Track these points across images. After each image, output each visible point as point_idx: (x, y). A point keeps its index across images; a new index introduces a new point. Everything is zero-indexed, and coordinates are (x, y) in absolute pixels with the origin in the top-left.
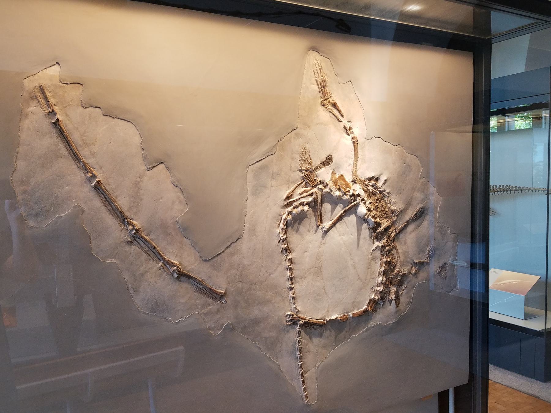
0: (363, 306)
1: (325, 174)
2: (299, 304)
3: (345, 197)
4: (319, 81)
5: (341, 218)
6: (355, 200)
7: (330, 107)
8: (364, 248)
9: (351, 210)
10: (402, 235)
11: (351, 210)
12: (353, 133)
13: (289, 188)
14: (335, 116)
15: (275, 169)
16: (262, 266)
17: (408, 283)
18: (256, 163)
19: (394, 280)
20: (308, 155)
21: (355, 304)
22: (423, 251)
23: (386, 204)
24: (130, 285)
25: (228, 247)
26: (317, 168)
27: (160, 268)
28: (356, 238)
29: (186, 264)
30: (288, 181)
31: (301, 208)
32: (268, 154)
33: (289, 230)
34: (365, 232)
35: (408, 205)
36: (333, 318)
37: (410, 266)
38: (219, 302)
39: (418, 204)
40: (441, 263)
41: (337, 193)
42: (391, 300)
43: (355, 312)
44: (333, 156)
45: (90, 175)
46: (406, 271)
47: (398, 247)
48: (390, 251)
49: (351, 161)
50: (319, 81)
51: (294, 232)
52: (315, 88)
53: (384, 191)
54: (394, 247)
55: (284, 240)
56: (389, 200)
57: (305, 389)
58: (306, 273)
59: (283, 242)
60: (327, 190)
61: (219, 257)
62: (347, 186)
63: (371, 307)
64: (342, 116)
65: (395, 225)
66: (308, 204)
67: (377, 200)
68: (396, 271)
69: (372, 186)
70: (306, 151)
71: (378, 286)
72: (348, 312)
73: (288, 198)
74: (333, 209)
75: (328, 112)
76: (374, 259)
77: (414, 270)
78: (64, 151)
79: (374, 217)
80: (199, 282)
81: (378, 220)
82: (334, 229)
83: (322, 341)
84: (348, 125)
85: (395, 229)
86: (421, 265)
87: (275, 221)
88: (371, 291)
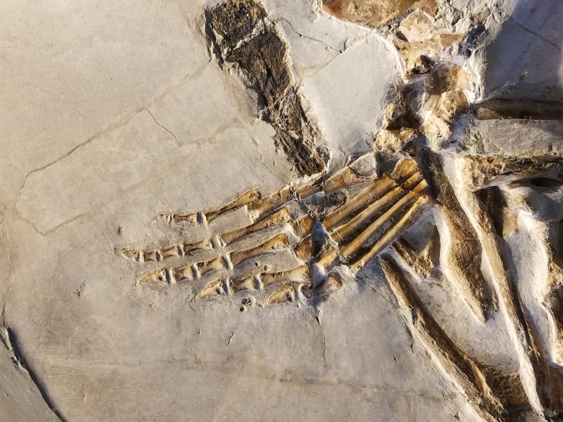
13: (438, 397)
20: (205, 233)
26: (302, 156)
30: (389, 399)
60: (470, 79)
70: (176, 242)
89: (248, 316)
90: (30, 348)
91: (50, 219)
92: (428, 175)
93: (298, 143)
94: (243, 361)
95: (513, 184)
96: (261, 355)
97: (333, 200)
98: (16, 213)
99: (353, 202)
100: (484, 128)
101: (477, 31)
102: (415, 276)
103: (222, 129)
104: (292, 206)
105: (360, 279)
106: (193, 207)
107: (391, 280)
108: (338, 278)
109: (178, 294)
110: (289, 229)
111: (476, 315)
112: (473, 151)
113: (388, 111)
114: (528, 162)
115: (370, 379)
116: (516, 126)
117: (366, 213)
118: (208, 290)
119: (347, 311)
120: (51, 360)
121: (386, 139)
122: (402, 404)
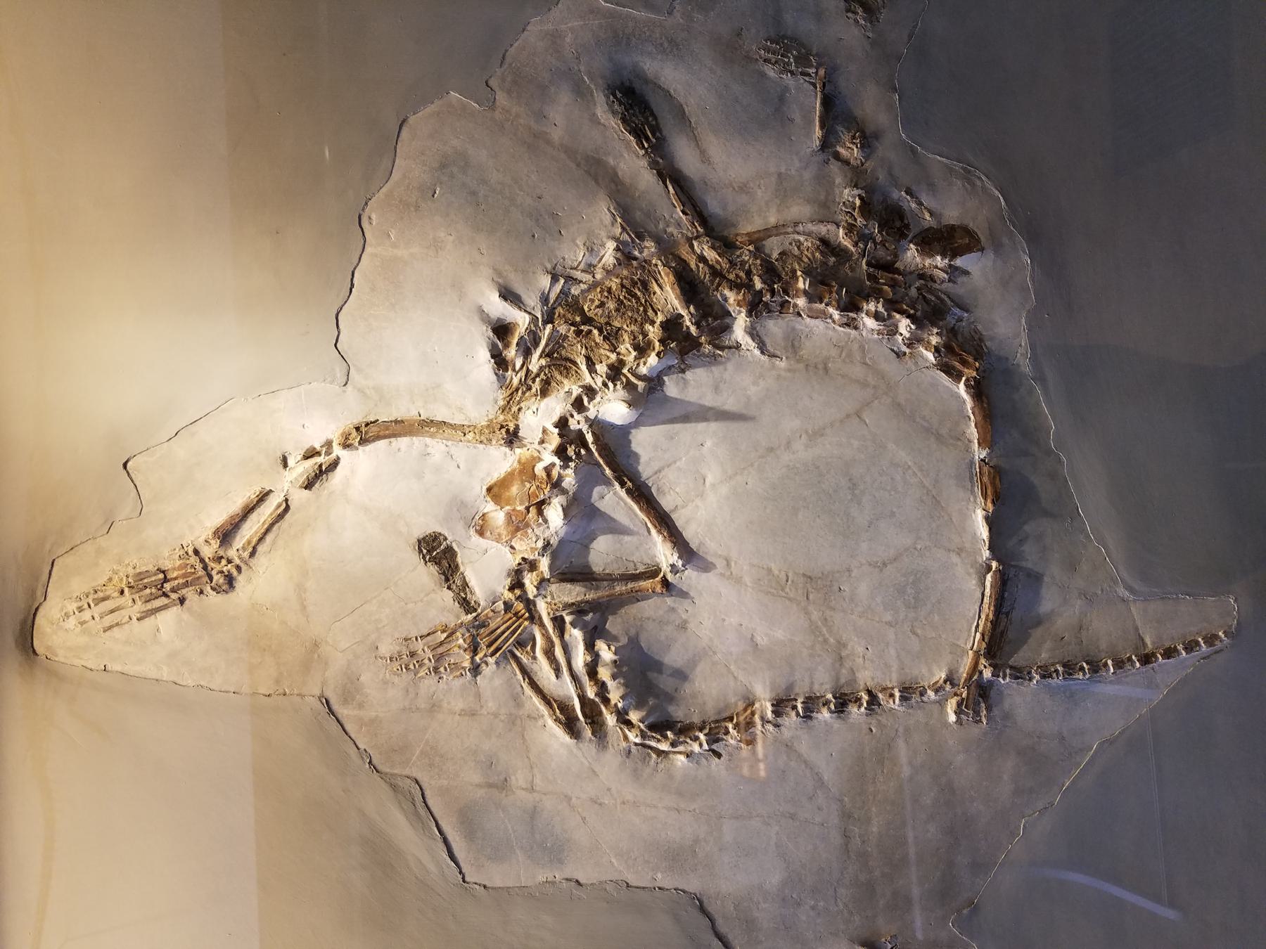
0: (958, 396)
1: (486, 567)
2: (924, 671)
3: (570, 480)
4: (140, 607)
5: (642, 495)
6: (580, 437)
7: (232, 553)
8: (753, 390)
9: (610, 454)
10: (713, 206)
11: (610, 454)
12: (329, 444)
14: (268, 531)
15: (472, 776)
16: (793, 817)
17: (897, 186)
18: (452, 856)
19: (881, 253)
20: (419, 646)
21: (944, 431)
26: (466, 605)
28: (713, 426)
30: (512, 720)
31: (604, 674)
32: (422, 811)
33: (678, 713)
34: (693, 385)
35: (598, 174)
36: (983, 532)
37: (834, 167)
39: (594, 120)
41: (554, 514)
42: (953, 271)
43: (973, 432)
44: (419, 532)
46: (850, 195)
48: (771, 272)
49: (436, 446)
50: (140, 607)
51: (687, 689)
52: (169, 620)
53: (545, 299)
54: (757, 240)
55: (713, 739)
56: (578, 274)
57: (1190, 647)
58: (826, 641)
60: (544, 564)
62: (526, 470)
63: (964, 363)
64: (263, 497)
65: (675, 244)
66: (590, 646)
67: (578, 333)
68: (847, 243)
69: (527, 353)
70: (405, 651)
71: (893, 331)
72: (972, 463)
73: (570, 725)
74: (615, 528)
75: (253, 562)
76: (793, 344)
77: (850, 151)
79: (642, 350)
81: (654, 332)
82: (679, 519)
83: (1054, 572)
84: (301, 469)
85: (689, 241)
86: (834, 112)
87: (648, 770)
88: (910, 363)
89: (442, 685)
90: (335, 707)
91: (344, 645)
92: (529, 611)
93: (465, 599)
94: (440, 707)
95: (571, 613)
96: (449, 703)
97: (483, 625)
98: (327, 642)
99: (493, 625)
100: (554, 587)
101: (547, 545)
102: (525, 659)
103: (427, 595)
104: (463, 630)
105: (497, 663)
106: (413, 634)
107: (515, 666)
108: (487, 664)
109: (407, 677)
110: (461, 641)
111: (553, 677)
112: (549, 599)
113: (508, 582)
114: (573, 604)
115: (503, 711)
116: (569, 586)
117: (499, 631)
118: (422, 674)
119: (491, 679)
120: (346, 712)
121: (508, 596)
122: (518, 722)
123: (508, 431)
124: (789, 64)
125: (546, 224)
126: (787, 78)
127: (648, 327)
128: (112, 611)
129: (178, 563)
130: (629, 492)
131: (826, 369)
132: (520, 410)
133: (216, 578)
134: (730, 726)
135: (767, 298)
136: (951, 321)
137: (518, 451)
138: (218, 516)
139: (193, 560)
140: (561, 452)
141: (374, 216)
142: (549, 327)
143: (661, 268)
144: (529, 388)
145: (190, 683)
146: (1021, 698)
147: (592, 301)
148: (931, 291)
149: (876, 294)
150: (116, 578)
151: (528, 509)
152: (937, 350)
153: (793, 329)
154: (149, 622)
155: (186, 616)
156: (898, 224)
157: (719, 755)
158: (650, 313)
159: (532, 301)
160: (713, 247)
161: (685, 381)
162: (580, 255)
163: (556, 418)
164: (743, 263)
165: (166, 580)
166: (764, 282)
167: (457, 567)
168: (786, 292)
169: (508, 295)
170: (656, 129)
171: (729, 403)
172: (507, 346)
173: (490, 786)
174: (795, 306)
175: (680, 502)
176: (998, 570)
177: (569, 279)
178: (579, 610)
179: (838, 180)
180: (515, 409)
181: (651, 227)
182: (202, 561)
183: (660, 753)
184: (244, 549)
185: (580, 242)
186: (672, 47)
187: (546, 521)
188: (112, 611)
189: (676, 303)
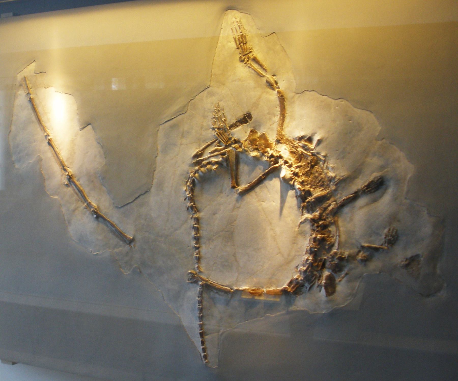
0: (283, 285)
10: (346, 210)
12: (278, 88)
13: (199, 146)
15: (186, 128)
22: (378, 234)
23: (322, 169)
24: (66, 217)
25: (137, 198)
26: (231, 127)
27: (85, 208)
29: (102, 207)
31: (209, 166)
32: (178, 114)
34: (292, 199)
37: (356, 250)
38: (128, 246)
40: (409, 253)
41: (254, 154)
42: (320, 286)
43: (272, 289)
45: (46, 134)
46: (346, 254)
47: (340, 223)
48: (325, 227)
52: (233, 45)
53: (318, 153)
56: (326, 164)
58: (214, 236)
59: (189, 199)
61: (129, 205)
62: (268, 145)
63: (293, 288)
64: (265, 70)
66: (217, 163)
67: (308, 163)
68: (332, 252)
74: (252, 170)
75: (247, 67)
76: (302, 233)
78: (34, 118)
79: (302, 183)
80: (112, 225)
81: (307, 188)
89: (210, 119)
99: (225, 134)
104: (224, 125)
105: (215, 135)
111: (210, 151)
113: (237, 139)
116: (235, 157)
121: (233, 139)
123: (280, 140)
124: (388, 237)
125: (342, 155)
126: (383, 236)
127: (309, 186)
128: (236, 30)
129: (248, 47)
130: (261, 177)
131: (294, 243)
132: (287, 144)
133: (243, 57)
134: (192, 204)
135: (316, 225)
136: (306, 284)
137: (274, 143)
138: (260, 57)
139: (248, 51)
140: (272, 156)
141: (343, 102)
142: (311, 154)
143: (327, 191)
144: (293, 147)
145: (216, 51)
146: (193, 293)
147: (318, 169)
148: (315, 279)
149: (315, 260)
150: (245, 31)
151: (257, 145)
152: (297, 279)
153: (307, 233)
154: (233, 40)
155: (234, 49)
156: (337, 269)
157: (185, 200)
158: (314, 187)
159: (318, 149)
160: (333, 209)
161: (293, 197)
162: (331, 165)
163: (282, 155)
164: (327, 218)
165: (244, 44)
166: (321, 225)
167: (242, 124)
168: (317, 231)
169: (319, 142)
170: (370, 192)
171: (285, 211)
172: (305, 141)
173: (183, 133)
174: (313, 234)
175: (257, 193)
176: (230, 291)
177: (325, 161)
178: (227, 160)
179: (352, 251)
180: (287, 143)
181: (340, 189)
182: (248, 54)
183: (187, 182)
184: (251, 65)
185: (335, 165)
186: (395, 199)
187: (253, 151)
188: (236, 30)
189: (315, 195)
